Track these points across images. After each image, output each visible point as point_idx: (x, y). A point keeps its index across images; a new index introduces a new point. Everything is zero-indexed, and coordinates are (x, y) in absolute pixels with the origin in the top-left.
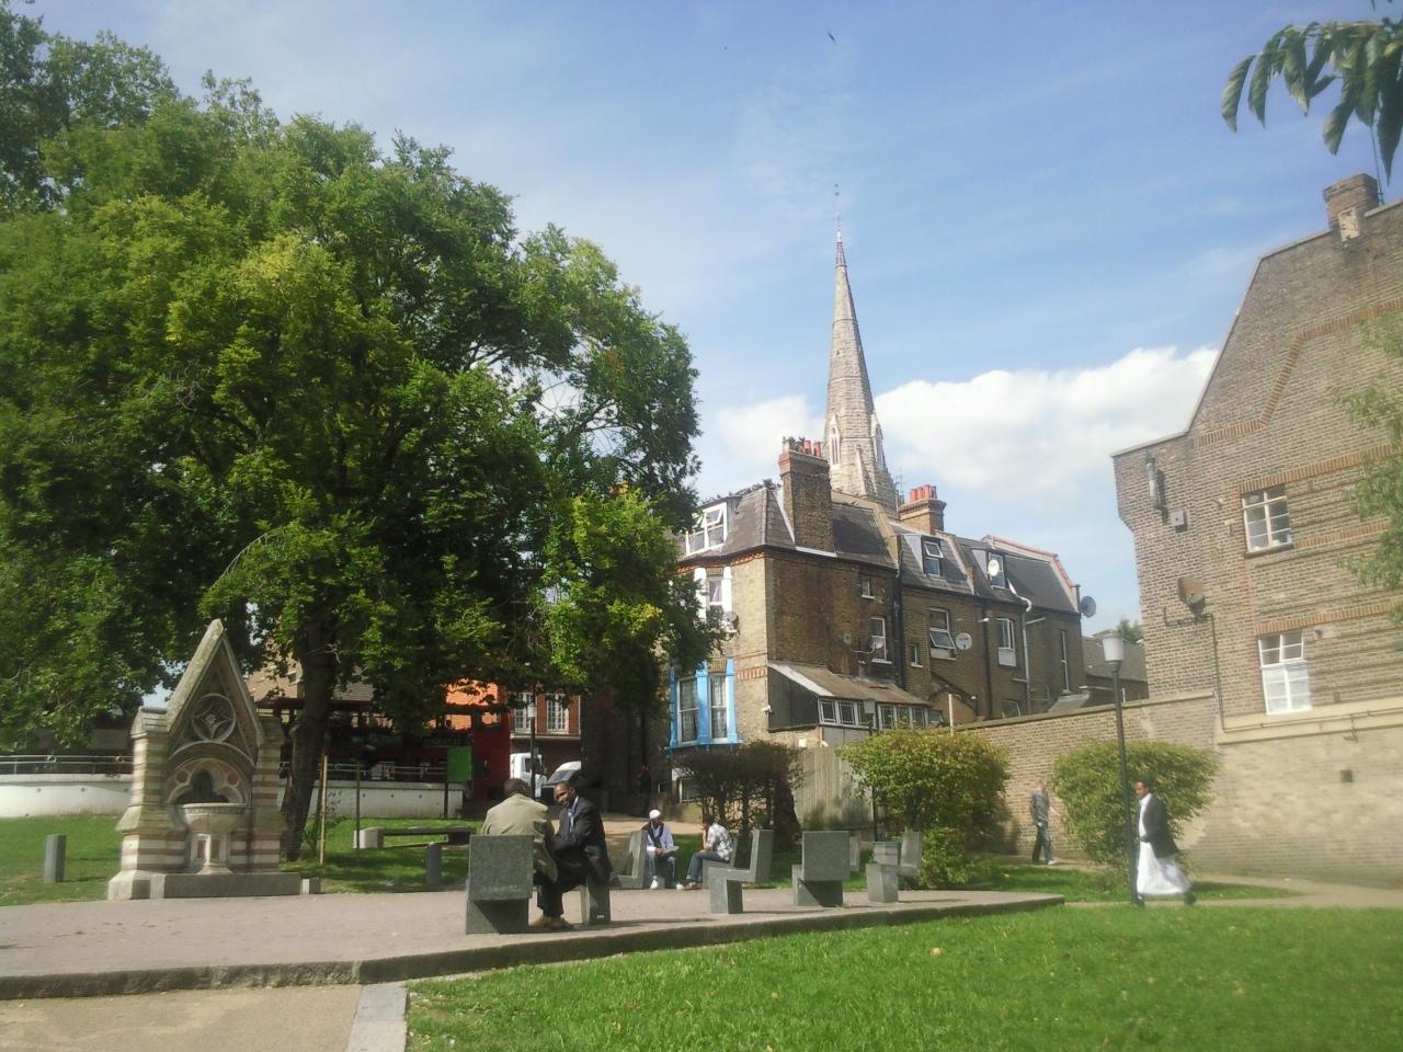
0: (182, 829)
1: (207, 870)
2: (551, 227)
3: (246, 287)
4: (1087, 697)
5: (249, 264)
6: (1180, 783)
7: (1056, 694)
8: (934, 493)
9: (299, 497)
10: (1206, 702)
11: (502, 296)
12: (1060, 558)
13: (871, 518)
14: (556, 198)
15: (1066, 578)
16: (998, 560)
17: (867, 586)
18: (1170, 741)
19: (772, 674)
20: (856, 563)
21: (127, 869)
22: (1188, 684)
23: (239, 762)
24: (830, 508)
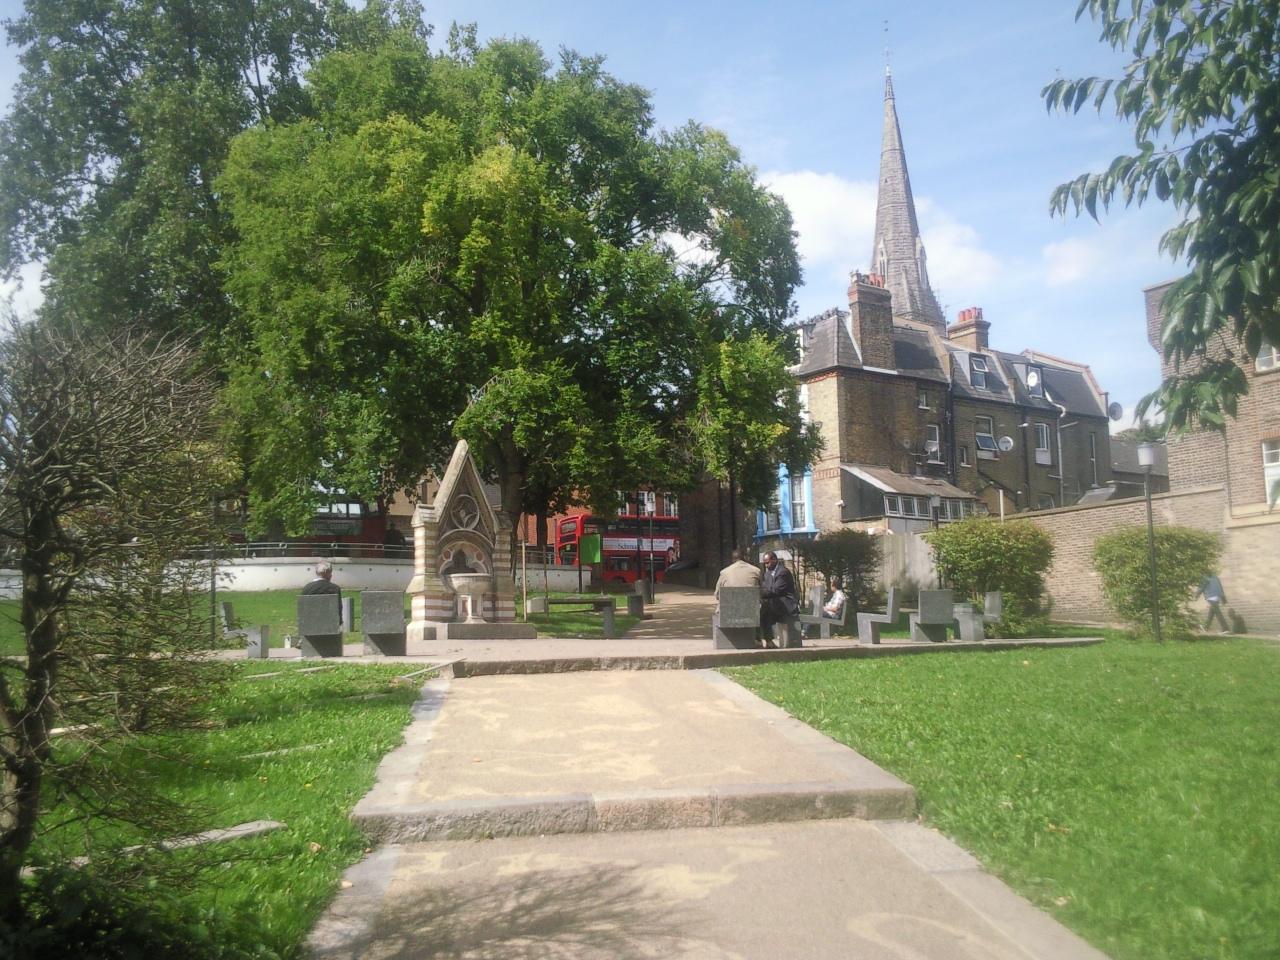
0: (451, 592)
1: (470, 620)
2: (691, 122)
3: (479, 190)
4: (1113, 490)
5: (476, 169)
6: (1194, 559)
7: (1086, 487)
8: (980, 314)
9: (520, 349)
10: (1217, 495)
11: (658, 185)
12: (1091, 369)
13: (926, 339)
14: (689, 100)
15: (1096, 387)
16: (1037, 372)
17: (923, 399)
18: (1187, 525)
19: (845, 475)
20: (915, 379)
21: (417, 620)
22: (1203, 479)
23: (483, 544)
24: (892, 332)
